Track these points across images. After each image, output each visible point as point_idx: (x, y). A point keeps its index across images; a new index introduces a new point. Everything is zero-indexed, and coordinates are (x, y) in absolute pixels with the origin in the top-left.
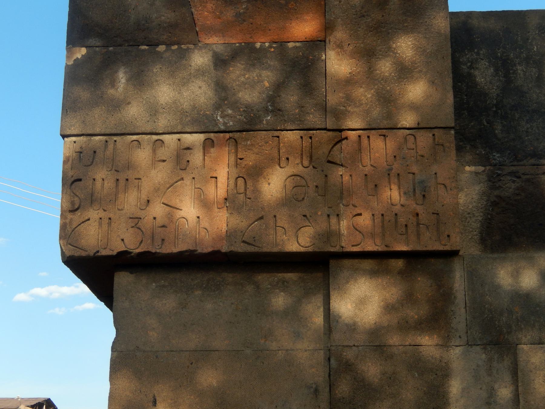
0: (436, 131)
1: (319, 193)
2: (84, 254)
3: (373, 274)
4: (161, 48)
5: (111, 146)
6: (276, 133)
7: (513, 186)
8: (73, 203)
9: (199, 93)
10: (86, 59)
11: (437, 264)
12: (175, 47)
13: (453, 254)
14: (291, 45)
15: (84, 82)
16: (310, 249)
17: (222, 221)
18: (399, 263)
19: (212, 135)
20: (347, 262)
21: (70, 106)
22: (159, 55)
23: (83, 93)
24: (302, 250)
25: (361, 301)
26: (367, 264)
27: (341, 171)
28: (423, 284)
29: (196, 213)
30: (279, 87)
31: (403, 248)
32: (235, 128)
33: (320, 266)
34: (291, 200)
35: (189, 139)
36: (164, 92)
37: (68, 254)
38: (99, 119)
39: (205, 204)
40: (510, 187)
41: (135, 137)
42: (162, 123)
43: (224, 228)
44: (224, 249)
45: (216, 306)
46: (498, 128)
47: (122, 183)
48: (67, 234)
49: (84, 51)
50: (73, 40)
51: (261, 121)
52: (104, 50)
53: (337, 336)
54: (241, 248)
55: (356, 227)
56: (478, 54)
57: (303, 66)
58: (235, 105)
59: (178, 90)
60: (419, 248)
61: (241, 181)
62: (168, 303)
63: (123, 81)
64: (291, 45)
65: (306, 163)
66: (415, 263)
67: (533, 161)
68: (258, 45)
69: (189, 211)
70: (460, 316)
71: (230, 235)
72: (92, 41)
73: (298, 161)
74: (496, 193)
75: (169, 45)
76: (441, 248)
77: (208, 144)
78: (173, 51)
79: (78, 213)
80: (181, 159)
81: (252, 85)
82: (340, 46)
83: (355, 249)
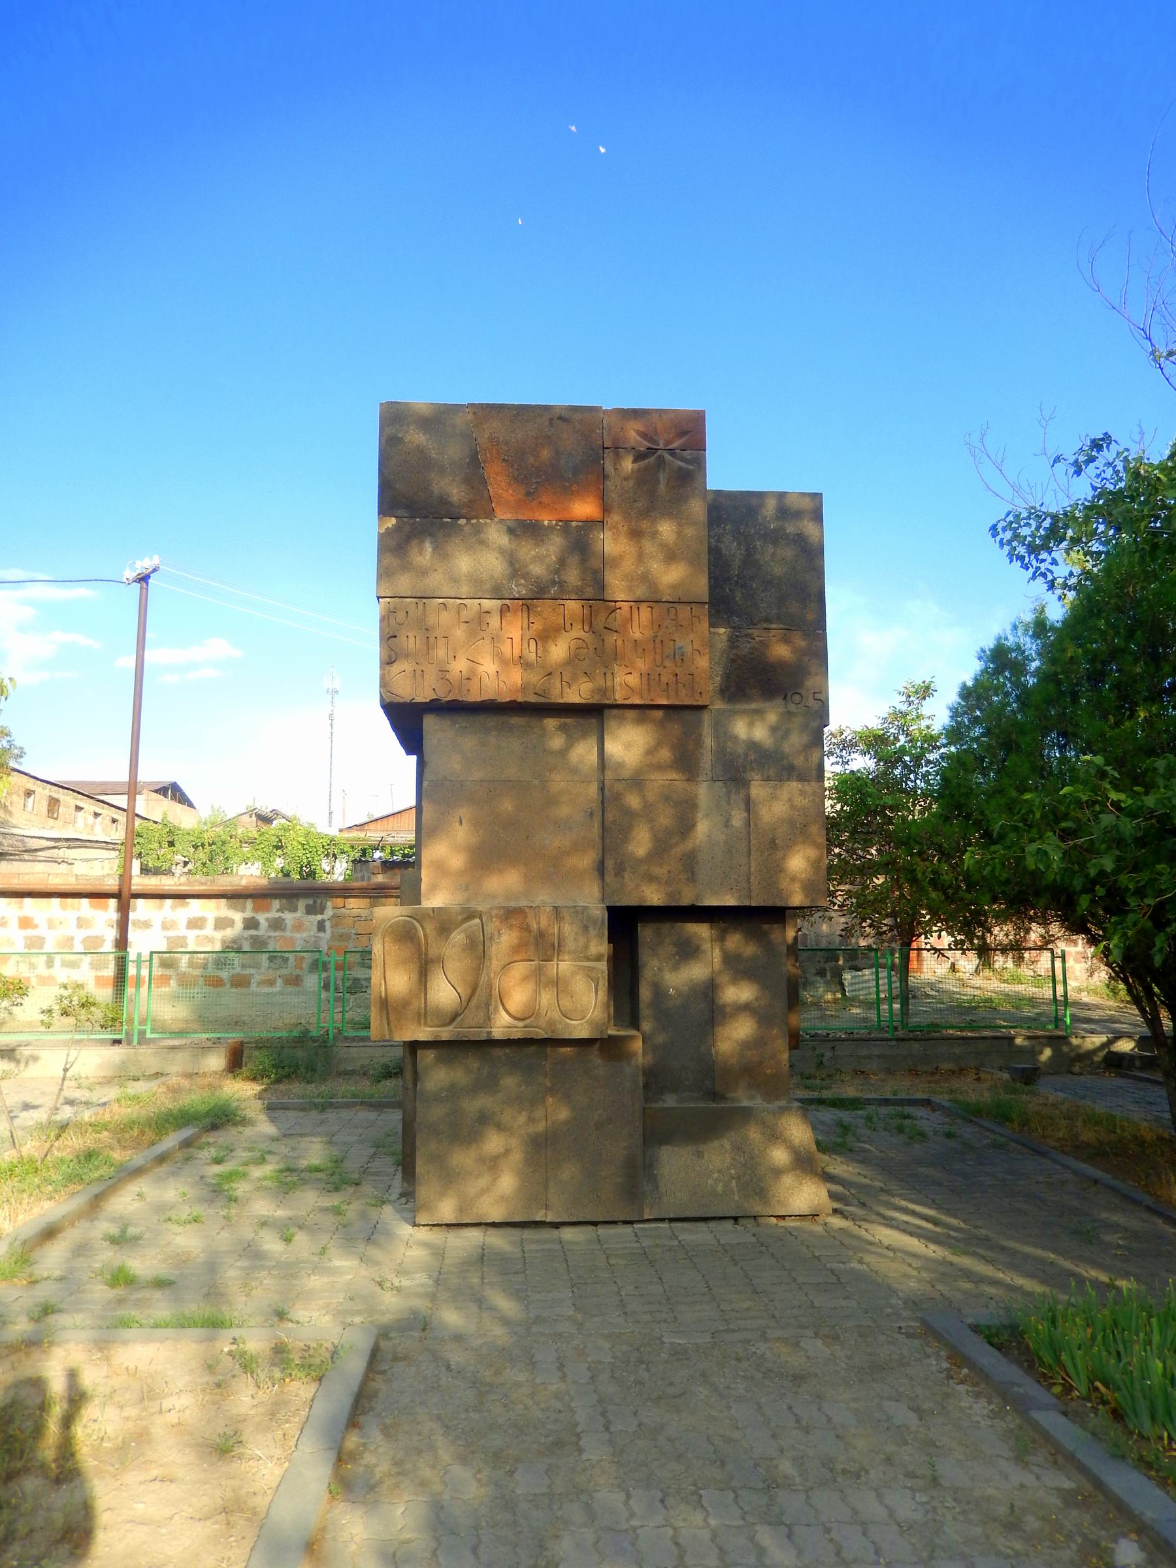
0: (693, 606)
1: (599, 656)
2: (401, 701)
3: (640, 721)
4: (462, 521)
5: (421, 607)
6: (562, 602)
7: (748, 646)
8: (390, 657)
9: (492, 564)
10: (397, 529)
11: (689, 716)
12: (474, 521)
13: (703, 707)
14: (574, 524)
15: (394, 549)
16: (590, 701)
17: (516, 677)
18: (659, 714)
19: (507, 602)
20: (615, 712)
21: (385, 574)
22: (461, 528)
23: (390, 559)
24: (583, 701)
25: (627, 744)
26: (631, 714)
27: (615, 636)
28: (675, 728)
29: (491, 666)
30: (562, 562)
31: (665, 702)
32: (530, 597)
33: (594, 714)
34: (572, 660)
35: (487, 604)
36: (464, 563)
37: (388, 700)
38: (404, 583)
39: (504, 662)
40: (745, 648)
41: (441, 601)
42: (465, 590)
43: (520, 682)
44: (520, 699)
45: (506, 746)
46: (738, 596)
47: (432, 640)
48: (384, 684)
49: (394, 520)
50: (385, 508)
51: (549, 592)
52: (412, 521)
53: (609, 775)
54: (533, 699)
55: (626, 682)
56: (724, 529)
57: (580, 541)
58: (526, 576)
59: (479, 559)
60: (677, 703)
61: (532, 643)
62: (469, 742)
63: (430, 550)
64: (574, 524)
65: (587, 629)
66: (676, 716)
67: (765, 625)
68: (546, 523)
69: (488, 667)
70: (707, 760)
71: (524, 688)
72: (400, 512)
73: (580, 626)
74: (734, 651)
75: (469, 519)
76: (695, 703)
77: (504, 610)
78: (473, 525)
79: (395, 666)
80: (479, 621)
81: (540, 558)
82: (614, 527)
83: (626, 702)
